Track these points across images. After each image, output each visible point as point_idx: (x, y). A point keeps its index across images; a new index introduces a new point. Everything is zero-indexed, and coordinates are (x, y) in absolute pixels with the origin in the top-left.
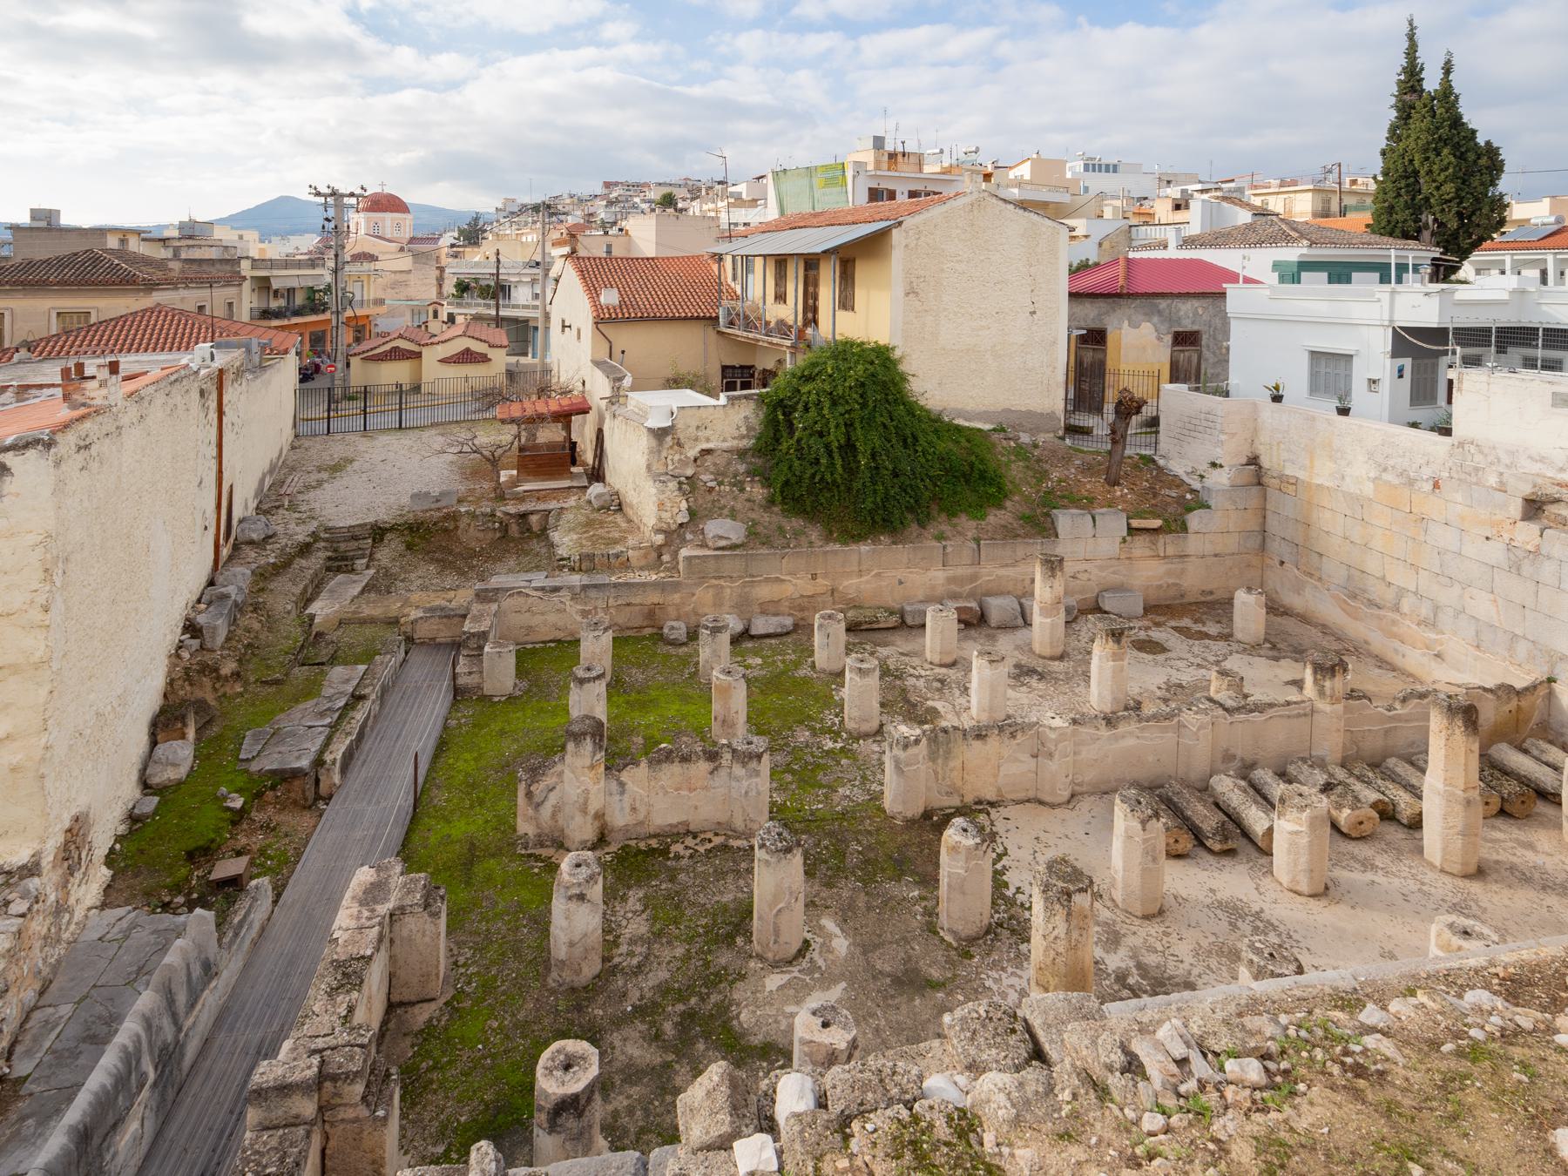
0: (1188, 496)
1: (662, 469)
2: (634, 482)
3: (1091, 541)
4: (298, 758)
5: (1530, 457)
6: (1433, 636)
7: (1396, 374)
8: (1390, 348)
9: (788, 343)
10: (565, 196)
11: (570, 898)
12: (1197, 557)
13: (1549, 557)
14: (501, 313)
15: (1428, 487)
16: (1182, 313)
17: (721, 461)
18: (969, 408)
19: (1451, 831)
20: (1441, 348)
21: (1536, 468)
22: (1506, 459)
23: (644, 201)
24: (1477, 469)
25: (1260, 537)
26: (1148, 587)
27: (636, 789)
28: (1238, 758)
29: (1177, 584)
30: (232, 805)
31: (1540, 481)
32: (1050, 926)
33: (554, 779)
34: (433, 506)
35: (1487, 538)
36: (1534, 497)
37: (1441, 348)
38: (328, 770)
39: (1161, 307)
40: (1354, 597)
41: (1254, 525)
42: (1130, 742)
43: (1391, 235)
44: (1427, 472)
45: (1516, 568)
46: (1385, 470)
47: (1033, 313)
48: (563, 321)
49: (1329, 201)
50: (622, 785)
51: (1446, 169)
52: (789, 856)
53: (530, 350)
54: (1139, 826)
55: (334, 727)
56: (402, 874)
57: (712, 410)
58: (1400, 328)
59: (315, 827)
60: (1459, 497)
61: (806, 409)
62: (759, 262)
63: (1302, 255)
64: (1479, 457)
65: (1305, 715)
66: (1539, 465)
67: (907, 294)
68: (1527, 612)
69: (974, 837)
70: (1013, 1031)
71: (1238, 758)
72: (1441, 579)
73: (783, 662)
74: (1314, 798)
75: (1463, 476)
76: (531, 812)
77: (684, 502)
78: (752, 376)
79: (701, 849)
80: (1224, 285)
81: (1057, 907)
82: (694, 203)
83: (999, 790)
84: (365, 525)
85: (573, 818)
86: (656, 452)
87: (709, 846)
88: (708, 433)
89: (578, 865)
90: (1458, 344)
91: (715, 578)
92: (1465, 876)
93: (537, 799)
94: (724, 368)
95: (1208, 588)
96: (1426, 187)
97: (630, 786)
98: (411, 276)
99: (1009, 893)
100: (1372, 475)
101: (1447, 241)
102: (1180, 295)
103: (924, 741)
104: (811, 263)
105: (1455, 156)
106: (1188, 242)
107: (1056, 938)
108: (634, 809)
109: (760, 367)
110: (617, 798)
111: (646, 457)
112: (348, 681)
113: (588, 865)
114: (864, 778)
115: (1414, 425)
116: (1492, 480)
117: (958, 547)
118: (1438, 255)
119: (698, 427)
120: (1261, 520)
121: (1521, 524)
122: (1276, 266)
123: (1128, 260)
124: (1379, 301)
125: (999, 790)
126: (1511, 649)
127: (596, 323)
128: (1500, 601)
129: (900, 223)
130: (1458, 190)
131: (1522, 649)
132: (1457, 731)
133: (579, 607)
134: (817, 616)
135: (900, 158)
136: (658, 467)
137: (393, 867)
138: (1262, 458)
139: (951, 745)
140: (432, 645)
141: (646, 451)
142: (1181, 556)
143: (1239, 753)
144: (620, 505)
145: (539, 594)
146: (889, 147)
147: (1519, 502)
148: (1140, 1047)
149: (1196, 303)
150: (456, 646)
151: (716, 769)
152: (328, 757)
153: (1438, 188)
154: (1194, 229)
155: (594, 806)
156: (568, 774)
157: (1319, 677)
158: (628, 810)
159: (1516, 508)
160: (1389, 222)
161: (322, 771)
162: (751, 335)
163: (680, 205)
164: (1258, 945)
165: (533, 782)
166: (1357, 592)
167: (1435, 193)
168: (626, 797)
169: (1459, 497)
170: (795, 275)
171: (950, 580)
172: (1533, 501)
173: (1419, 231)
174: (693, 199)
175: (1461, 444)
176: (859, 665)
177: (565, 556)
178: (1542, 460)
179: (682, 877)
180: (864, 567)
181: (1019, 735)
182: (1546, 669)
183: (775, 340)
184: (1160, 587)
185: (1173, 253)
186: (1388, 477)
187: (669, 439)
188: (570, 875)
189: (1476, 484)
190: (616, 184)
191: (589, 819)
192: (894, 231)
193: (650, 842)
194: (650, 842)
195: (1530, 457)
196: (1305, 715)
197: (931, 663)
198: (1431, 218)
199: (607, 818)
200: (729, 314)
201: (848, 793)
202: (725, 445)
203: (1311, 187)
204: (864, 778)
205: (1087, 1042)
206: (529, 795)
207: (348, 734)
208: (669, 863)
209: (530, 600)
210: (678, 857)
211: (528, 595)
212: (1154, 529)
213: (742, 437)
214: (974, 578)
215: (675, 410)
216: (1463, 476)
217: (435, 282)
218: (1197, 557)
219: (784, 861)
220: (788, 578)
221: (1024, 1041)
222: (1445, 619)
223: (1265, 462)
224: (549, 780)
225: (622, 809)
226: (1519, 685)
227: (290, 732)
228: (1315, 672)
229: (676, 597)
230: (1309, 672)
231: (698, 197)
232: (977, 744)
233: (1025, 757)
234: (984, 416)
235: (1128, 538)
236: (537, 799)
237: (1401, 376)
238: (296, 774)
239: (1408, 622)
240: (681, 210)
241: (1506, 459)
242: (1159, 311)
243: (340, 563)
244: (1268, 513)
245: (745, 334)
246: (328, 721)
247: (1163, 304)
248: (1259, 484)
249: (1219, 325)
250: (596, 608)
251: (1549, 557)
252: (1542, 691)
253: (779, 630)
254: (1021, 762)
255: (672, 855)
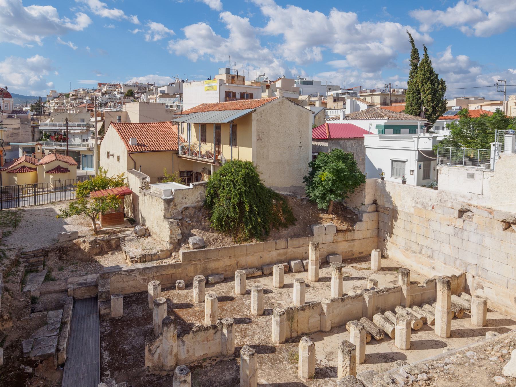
0: (354, 217)
1: (169, 216)
2: (157, 222)
3: (324, 236)
4: (50, 349)
5: (461, 196)
6: (432, 261)
7: (419, 168)
8: (417, 158)
9: (212, 161)
10: (81, 90)
11: (181, 382)
12: (358, 240)
13: (466, 230)
14: (69, 149)
15: (430, 208)
16: (348, 146)
17: (192, 212)
18: (279, 186)
19: (443, 323)
20: (434, 158)
21: (461, 200)
22: (454, 197)
23: (118, 93)
24: (445, 201)
25: (377, 231)
26: (343, 252)
27: (188, 343)
28: (380, 308)
29: (352, 251)
30: (28, 371)
31: (463, 204)
32: (345, 363)
33: (159, 343)
34: (68, 239)
35: (448, 225)
36: (461, 210)
37: (434, 158)
38: (62, 353)
39: (341, 143)
40: (408, 250)
41: (375, 227)
42: (349, 306)
43: (411, 114)
44: (430, 203)
45: (456, 235)
46: (417, 203)
47: (301, 147)
48: (108, 153)
49: (386, 98)
50: (183, 342)
51: (429, 89)
52: (253, 356)
53: (81, 166)
54: (359, 332)
55: (59, 335)
56: (116, 383)
57: (187, 190)
58: (421, 151)
59: (62, 375)
60: (440, 211)
61: (224, 189)
62: (192, 125)
63: (385, 123)
64: (446, 197)
65: (399, 291)
66: (463, 199)
67: (258, 140)
68: (459, 249)
69: (310, 342)
70: (357, 382)
71: (380, 308)
72: (434, 241)
73: (223, 292)
74: (407, 317)
75: (441, 204)
76: (150, 357)
77: (180, 230)
78: (192, 175)
79: (214, 363)
80: (364, 135)
81: (347, 356)
82: (143, 95)
83: (309, 329)
84: (39, 250)
85: (167, 357)
86: (166, 209)
87: (216, 362)
88: (186, 200)
89: (182, 370)
90: (440, 157)
91: (194, 261)
92: (447, 338)
93: (153, 352)
94: (181, 172)
95: (361, 251)
96: (422, 96)
97: (186, 342)
98: (20, 131)
99: (318, 362)
100: (413, 205)
101: (429, 117)
102: (347, 139)
103: (286, 313)
104: (218, 127)
105: (431, 84)
106: (346, 117)
107: (346, 367)
108: (188, 351)
109: (195, 171)
110: (182, 347)
111: (163, 212)
112: (57, 317)
113: (185, 369)
114: (263, 331)
115: (424, 186)
116: (449, 205)
117: (282, 243)
118: (426, 122)
119: (182, 198)
120: (377, 224)
121: (458, 219)
122: (377, 127)
123: (328, 124)
124: (414, 141)
125: (309, 329)
126: (455, 263)
127: (129, 154)
128: (451, 246)
129: (255, 110)
130: (433, 97)
131: (458, 262)
132: (445, 290)
133: (142, 277)
134: (236, 272)
135: (236, 77)
136: (168, 215)
137: (112, 381)
138: (378, 201)
139: (294, 314)
140: (85, 300)
141: (163, 209)
142: (353, 240)
143: (381, 307)
144: (149, 233)
145: (126, 273)
146: (233, 73)
147: (457, 212)
148: (395, 376)
149: (352, 141)
150: (95, 299)
151: (216, 332)
152: (61, 348)
153: (426, 96)
154: (348, 111)
155: (175, 351)
156: (164, 340)
157: (403, 277)
158: (186, 352)
159: (456, 214)
160: (411, 109)
161: (59, 353)
162: (194, 158)
163: (136, 96)
164: (399, 363)
165: (151, 345)
166: (409, 248)
167: (425, 98)
168: (185, 347)
169: (440, 211)
170: (211, 133)
171: (279, 255)
172: (461, 211)
173: (420, 113)
174: (142, 93)
175: (441, 192)
176: (257, 289)
177: (134, 256)
178: (464, 197)
179: (209, 374)
180: (248, 252)
181: (315, 307)
182: (464, 268)
183: (206, 160)
184: (346, 252)
185: (342, 121)
186: (418, 205)
187: (172, 203)
188: (180, 374)
189: (445, 206)
190: (105, 85)
191: (173, 356)
192: (253, 114)
193: (194, 363)
194: (194, 363)
195: (461, 196)
196: (399, 291)
197: (276, 287)
198: (424, 108)
199: (179, 356)
200: (183, 149)
201: (259, 337)
202: (193, 205)
203: (380, 93)
204: (263, 331)
205: (380, 379)
206: (150, 350)
207: (65, 338)
208: (203, 370)
209: (122, 276)
210: (206, 367)
211: (121, 274)
212: (345, 230)
213: (199, 202)
214: (285, 254)
215: (173, 191)
216: (441, 204)
217: (31, 133)
218: (358, 240)
219: (252, 359)
220: (221, 258)
221: (361, 384)
222: (436, 255)
223: (379, 202)
224: (157, 343)
225: (184, 352)
226: (457, 275)
227: (41, 339)
228: (402, 276)
229: (180, 270)
230: (400, 276)
231: (145, 92)
232: (302, 312)
233: (317, 316)
234: (285, 189)
235: (336, 234)
236: (153, 352)
237: (420, 169)
238: (50, 355)
239: (424, 257)
240: (137, 98)
241: (454, 197)
242: (340, 145)
243: (32, 269)
244: (380, 222)
245: (201, 159)
246: (56, 333)
247: (342, 142)
248: (377, 211)
249: (359, 150)
250: (149, 277)
251: (466, 230)
252: (463, 276)
253: (219, 280)
254: (316, 317)
255: (204, 367)
